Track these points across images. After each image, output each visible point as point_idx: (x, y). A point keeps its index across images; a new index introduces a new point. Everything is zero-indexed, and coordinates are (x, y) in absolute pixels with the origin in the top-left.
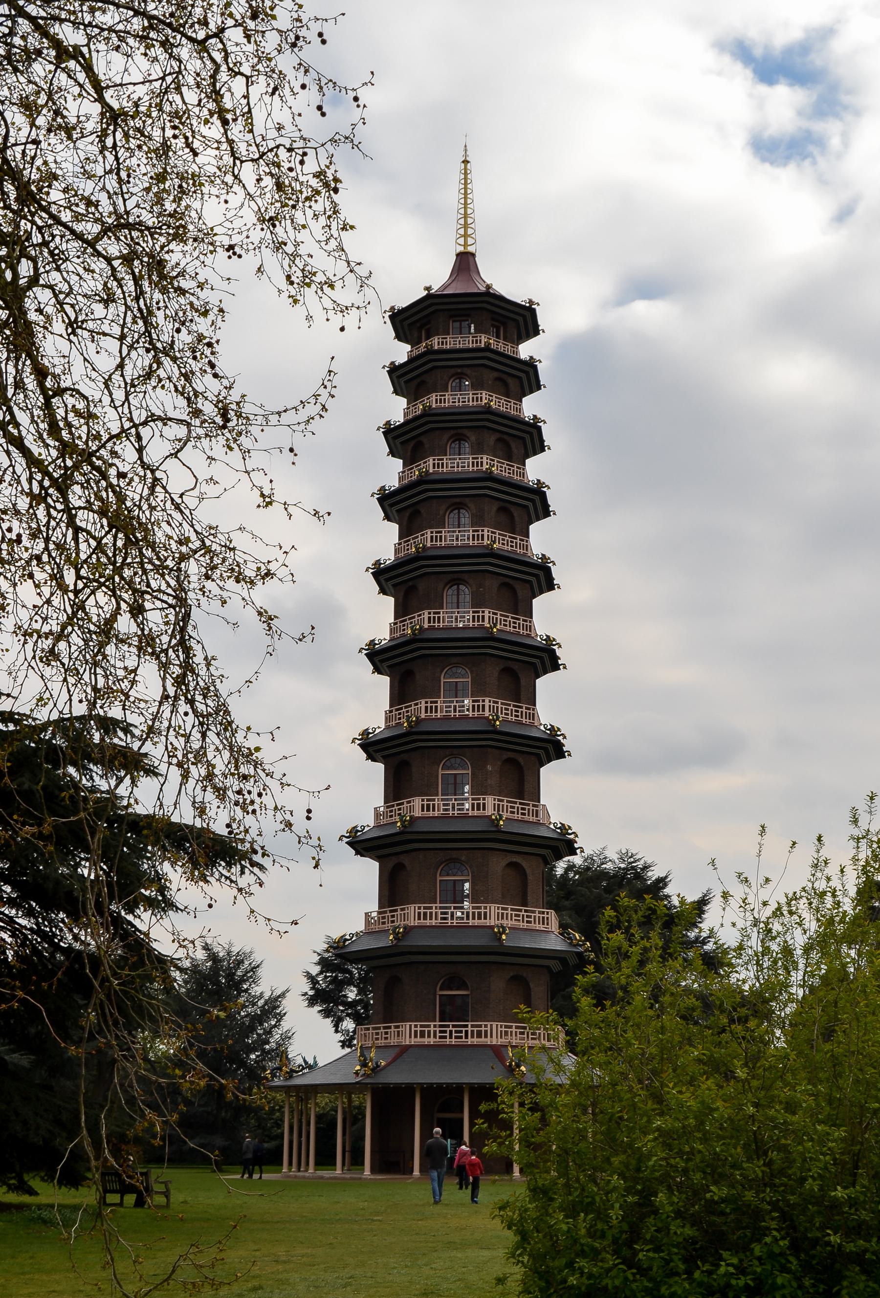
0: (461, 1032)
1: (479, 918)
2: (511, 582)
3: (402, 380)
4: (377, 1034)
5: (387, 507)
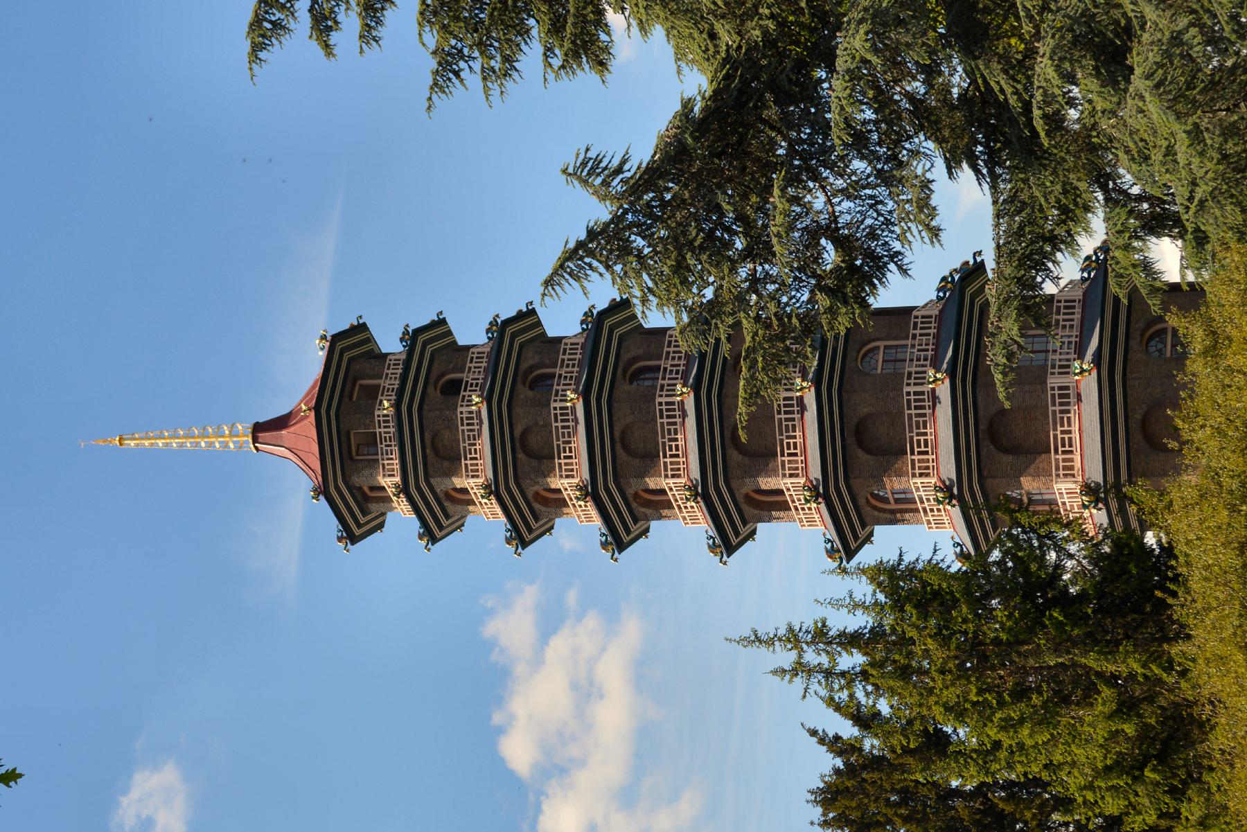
0: (787, 426)
1: (1068, 396)
2: (621, 365)
3: (445, 522)
4: (932, 510)
5: (632, 536)
